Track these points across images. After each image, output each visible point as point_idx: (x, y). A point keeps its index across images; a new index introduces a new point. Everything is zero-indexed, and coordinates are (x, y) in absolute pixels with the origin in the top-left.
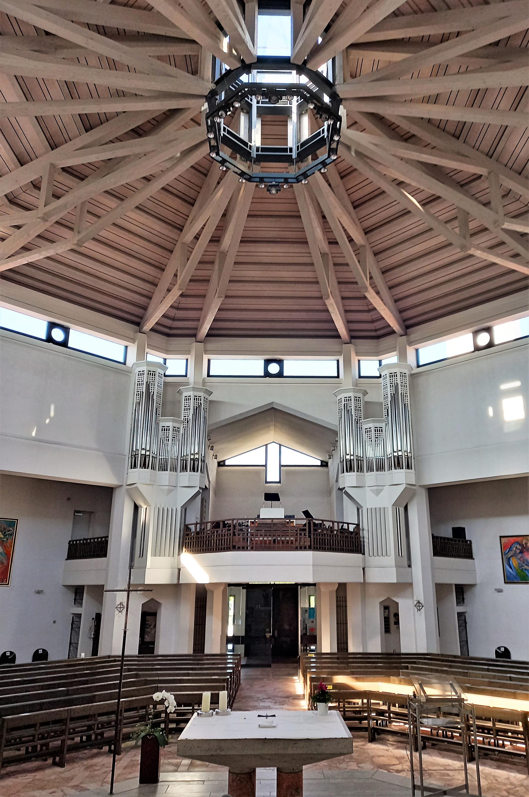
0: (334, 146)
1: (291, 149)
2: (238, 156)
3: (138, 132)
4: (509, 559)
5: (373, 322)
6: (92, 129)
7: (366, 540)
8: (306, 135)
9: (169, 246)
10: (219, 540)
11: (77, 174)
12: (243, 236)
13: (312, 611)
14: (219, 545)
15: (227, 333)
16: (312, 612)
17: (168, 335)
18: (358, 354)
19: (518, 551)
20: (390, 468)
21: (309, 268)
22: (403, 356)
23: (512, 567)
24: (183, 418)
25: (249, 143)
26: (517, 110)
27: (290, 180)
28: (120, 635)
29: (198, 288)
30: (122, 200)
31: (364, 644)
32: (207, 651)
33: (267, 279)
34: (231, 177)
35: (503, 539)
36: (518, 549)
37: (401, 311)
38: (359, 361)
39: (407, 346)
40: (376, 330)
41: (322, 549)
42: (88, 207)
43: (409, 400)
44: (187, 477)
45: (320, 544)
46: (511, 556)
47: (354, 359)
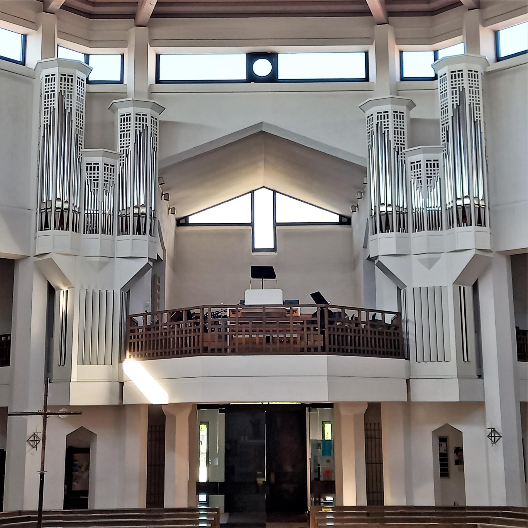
7: (411, 337)
17: (433, 13)
18: (399, 41)
20: (450, 224)
31: (409, 494)
32: (167, 504)
38: (401, 52)
47: (394, 50)
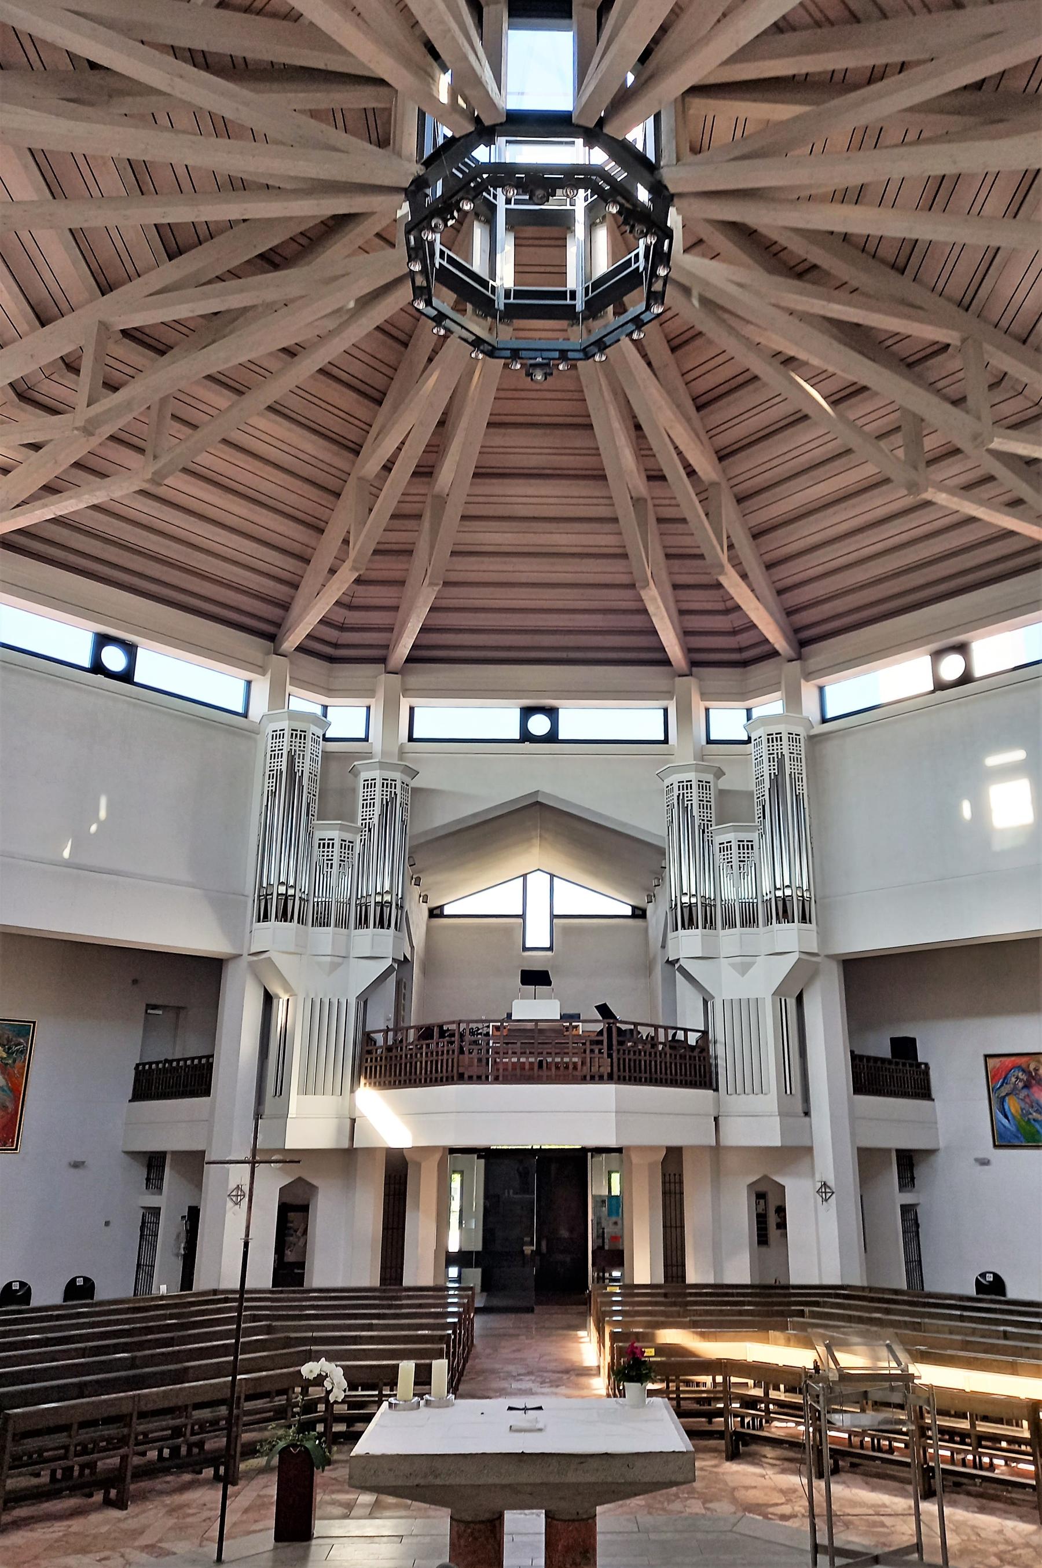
0: (658, 286)
1: (573, 294)
2: (469, 307)
3: (272, 260)
4: (1002, 1100)
5: (734, 633)
6: (181, 253)
7: (721, 1062)
8: (602, 266)
9: (332, 483)
10: (432, 1062)
11: (151, 342)
12: (480, 465)
13: (614, 1202)
14: (431, 1072)
15: (447, 655)
16: (614, 1205)
17: (332, 659)
18: (704, 696)
19: (1021, 1085)
20: (768, 921)
21: (608, 527)
22: (793, 700)
23: (1009, 1115)
24: (360, 822)
25: (491, 282)
26: (1018, 217)
27: (570, 355)
28: (236, 1249)
29: (389, 567)
30: (240, 393)
31: (718, 1267)
32: (407, 1282)
33: (526, 549)
34: (455, 347)
35: (990, 1061)
36: (1021, 1080)
37: (789, 613)
38: (707, 710)
39: (803, 681)
40: (740, 650)
41: (635, 1080)
42: (174, 406)
43: (805, 787)
44: (369, 939)
45: (630, 1071)
46: (1007, 1095)
47: (698, 707)
